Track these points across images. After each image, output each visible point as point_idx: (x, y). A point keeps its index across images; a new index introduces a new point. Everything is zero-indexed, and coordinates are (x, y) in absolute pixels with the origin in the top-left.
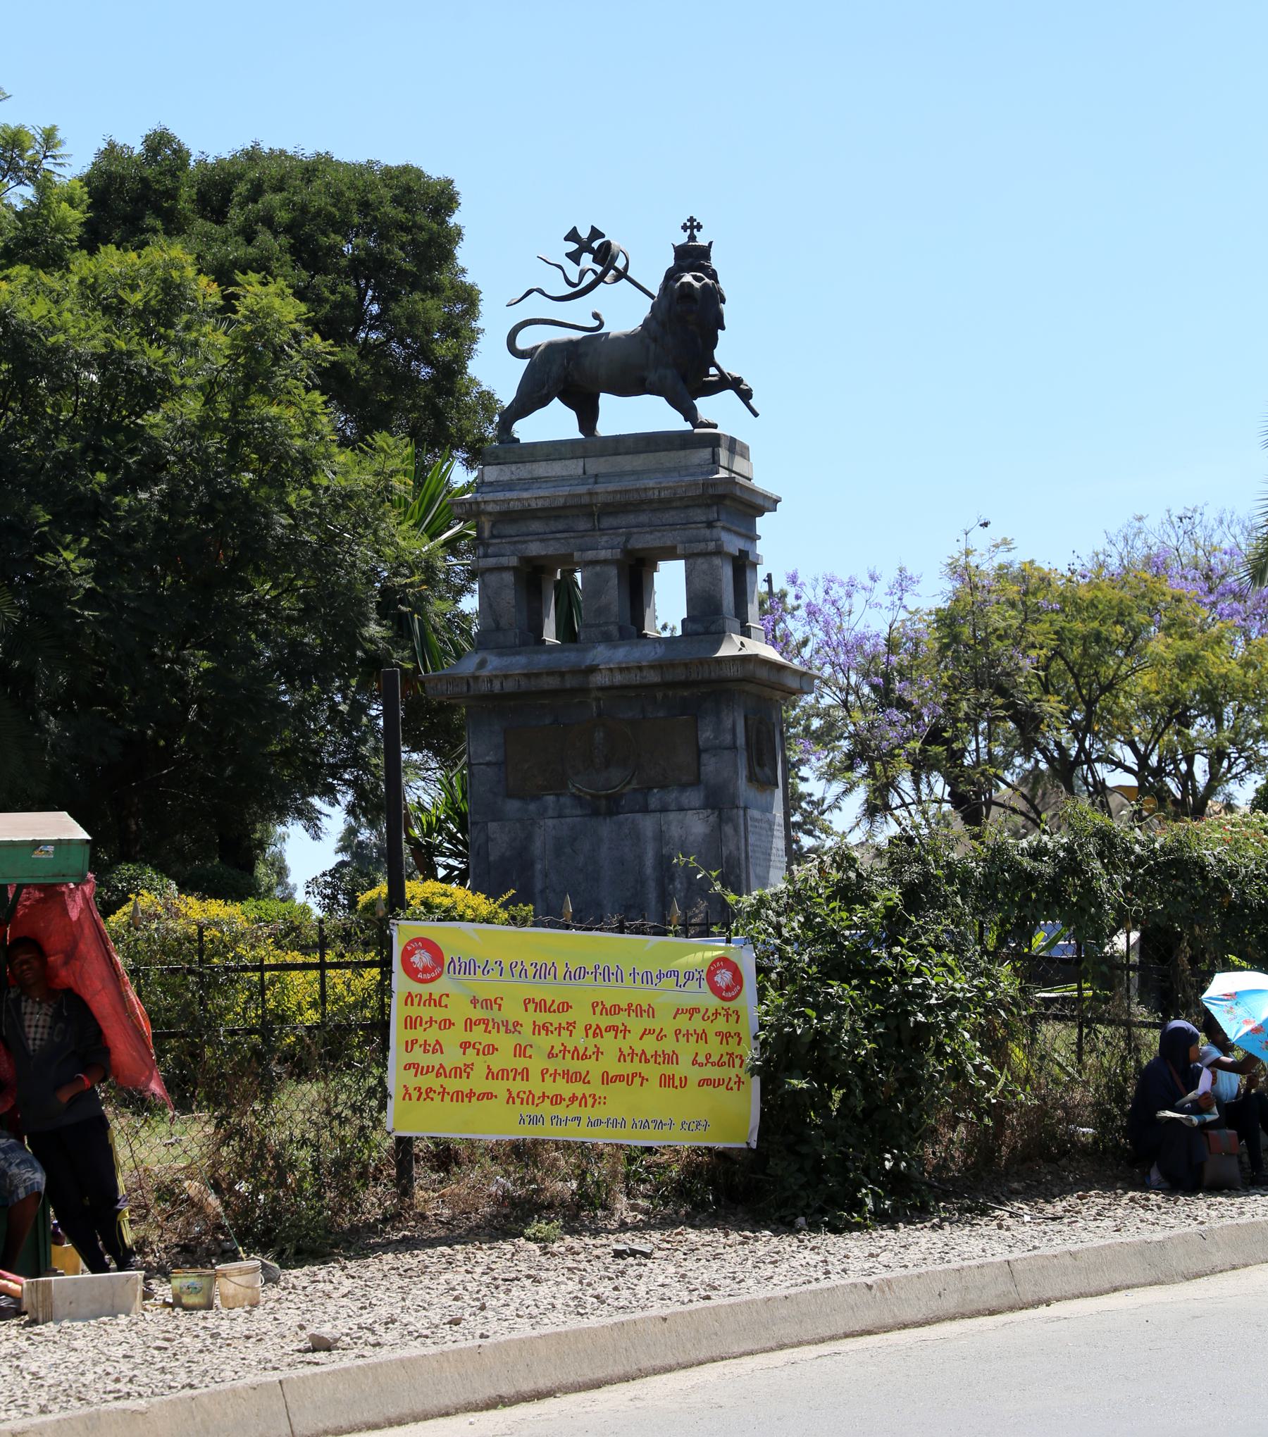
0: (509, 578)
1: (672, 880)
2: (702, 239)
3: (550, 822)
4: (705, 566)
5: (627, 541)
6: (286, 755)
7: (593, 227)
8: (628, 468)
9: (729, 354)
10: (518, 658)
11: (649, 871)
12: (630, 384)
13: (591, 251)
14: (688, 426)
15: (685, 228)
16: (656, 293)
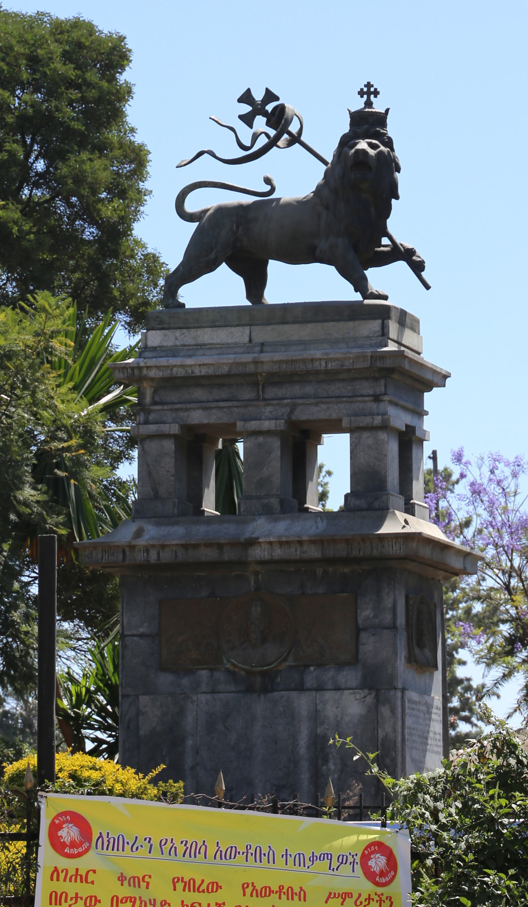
0: (169, 445)
1: (326, 761)
3: (203, 698)
4: (370, 441)
5: (291, 412)
7: (267, 90)
8: (295, 338)
9: (402, 224)
10: (176, 528)
11: (302, 750)
13: (265, 114)
14: (358, 297)
15: (361, 93)
16: (329, 159)
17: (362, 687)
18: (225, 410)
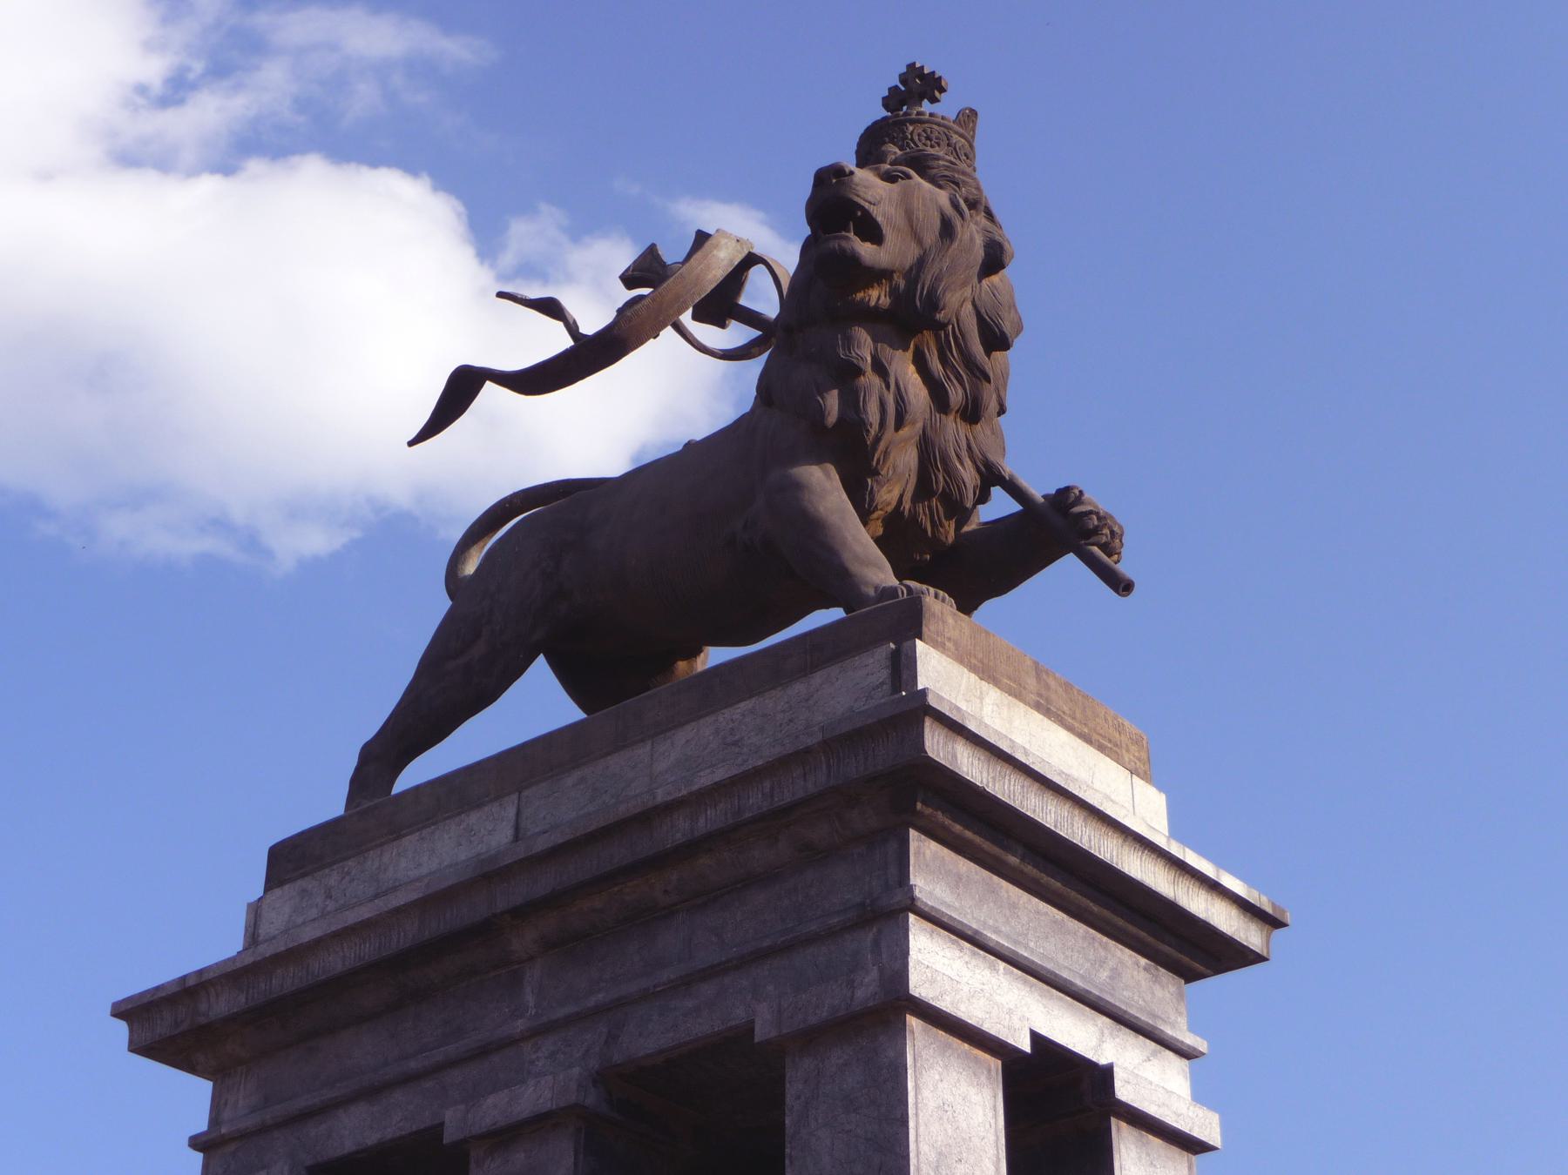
18: (428, 1084)
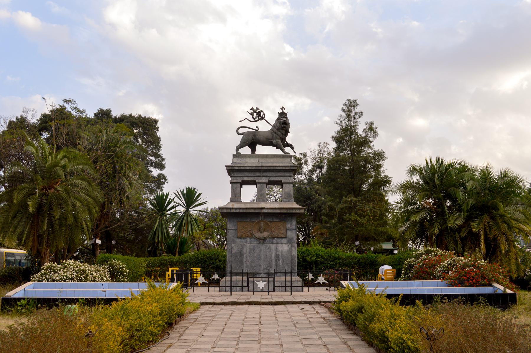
1: (279, 260)
2: (285, 111)
3: (248, 245)
6: (180, 228)
9: (289, 139)
11: (273, 258)
12: (267, 143)
13: (256, 113)
14: (283, 153)
17: (287, 243)
